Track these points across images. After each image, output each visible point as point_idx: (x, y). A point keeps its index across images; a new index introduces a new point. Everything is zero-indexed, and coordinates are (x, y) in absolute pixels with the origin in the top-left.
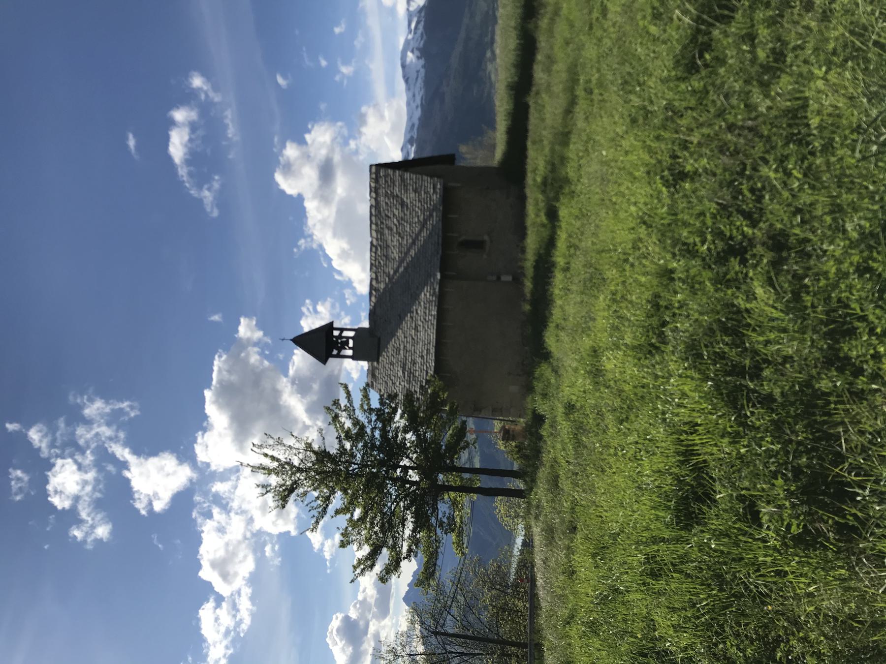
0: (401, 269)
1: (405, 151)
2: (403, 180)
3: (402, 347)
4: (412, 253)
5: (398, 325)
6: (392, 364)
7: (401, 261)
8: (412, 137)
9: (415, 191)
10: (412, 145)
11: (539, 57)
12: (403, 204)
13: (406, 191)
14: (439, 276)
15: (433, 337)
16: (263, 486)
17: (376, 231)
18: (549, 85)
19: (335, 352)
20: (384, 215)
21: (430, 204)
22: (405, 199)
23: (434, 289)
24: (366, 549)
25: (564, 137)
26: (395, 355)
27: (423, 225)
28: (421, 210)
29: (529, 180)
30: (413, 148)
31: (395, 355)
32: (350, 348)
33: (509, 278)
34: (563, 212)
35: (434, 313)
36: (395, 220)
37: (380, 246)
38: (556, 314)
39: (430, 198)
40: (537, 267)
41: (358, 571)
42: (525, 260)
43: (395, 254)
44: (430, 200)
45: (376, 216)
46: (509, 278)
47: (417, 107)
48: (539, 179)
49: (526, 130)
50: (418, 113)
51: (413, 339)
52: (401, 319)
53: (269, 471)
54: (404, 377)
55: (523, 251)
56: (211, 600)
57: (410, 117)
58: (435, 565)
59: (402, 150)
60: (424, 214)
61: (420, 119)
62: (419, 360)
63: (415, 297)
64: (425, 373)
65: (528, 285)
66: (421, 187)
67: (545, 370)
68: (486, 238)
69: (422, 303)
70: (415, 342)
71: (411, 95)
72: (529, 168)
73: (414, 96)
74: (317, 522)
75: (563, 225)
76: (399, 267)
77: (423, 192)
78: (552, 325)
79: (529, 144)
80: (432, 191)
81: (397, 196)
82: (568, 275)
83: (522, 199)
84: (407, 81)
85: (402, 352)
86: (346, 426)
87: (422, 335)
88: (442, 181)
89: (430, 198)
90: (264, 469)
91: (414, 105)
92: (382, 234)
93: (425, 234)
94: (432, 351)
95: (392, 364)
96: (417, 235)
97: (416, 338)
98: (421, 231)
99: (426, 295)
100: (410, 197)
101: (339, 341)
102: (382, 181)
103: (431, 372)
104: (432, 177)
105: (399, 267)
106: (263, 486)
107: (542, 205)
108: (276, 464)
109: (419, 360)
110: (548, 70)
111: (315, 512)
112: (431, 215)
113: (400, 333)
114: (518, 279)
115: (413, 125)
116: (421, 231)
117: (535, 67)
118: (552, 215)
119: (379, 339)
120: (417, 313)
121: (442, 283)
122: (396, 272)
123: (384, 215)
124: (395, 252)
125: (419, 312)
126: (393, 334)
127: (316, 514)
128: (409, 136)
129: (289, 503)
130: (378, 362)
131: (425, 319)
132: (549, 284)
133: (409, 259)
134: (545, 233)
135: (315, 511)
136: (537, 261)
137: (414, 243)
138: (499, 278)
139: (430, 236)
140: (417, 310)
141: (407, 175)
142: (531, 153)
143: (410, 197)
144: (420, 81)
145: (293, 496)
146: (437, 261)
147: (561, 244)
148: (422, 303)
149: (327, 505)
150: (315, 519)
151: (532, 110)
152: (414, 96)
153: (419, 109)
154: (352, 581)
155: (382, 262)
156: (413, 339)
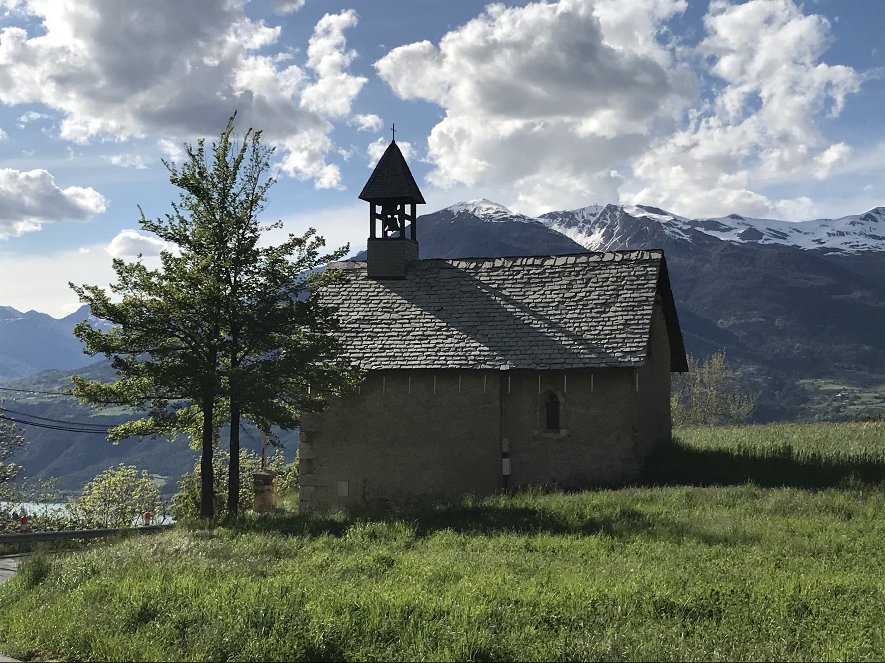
0: (510, 308)
1: (730, 223)
2: (641, 303)
3: (394, 316)
4: (537, 324)
5: (425, 307)
6: (367, 301)
7: (523, 308)
8: (760, 235)
9: (626, 324)
10: (742, 236)
11: (800, 495)
12: (607, 305)
13: (625, 310)
14: (503, 368)
15: (414, 365)
16: (200, 150)
17: (566, 264)
18: (758, 511)
19: (379, 210)
20: (589, 276)
21: (608, 348)
22: (613, 309)
23: (485, 362)
24: (116, 299)
25: (679, 532)
26: (382, 305)
27: (578, 338)
28: (599, 334)
29: (642, 493)
30: (737, 239)
31: (382, 305)
32: (385, 233)
33: (506, 470)
34: (593, 540)
35: (451, 364)
36: (583, 294)
37: (544, 272)
38: (478, 541)
39: (617, 348)
40: (529, 513)
41: (87, 293)
42: (535, 496)
43: (533, 297)
44: (613, 348)
45: (588, 263)
46: (506, 470)
47: (819, 241)
48: (638, 507)
49: (706, 484)
50: (807, 244)
51: (409, 332)
52: (438, 312)
53: (221, 159)
54: (349, 323)
55: (547, 491)
56: (120, 157)
57: (797, 229)
58: (108, 402)
59: (734, 217)
60: (592, 340)
61: (796, 247)
62: (378, 344)
63: (471, 332)
64: (361, 355)
65: (503, 502)
66: (633, 333)
67: (406, 533)
68: (563, 432)
69: (462, 344)
70: (403, 336)
71: (842, 227)
72: (656, 491)
73: (842, 234)
74: (155, 229)
75: (579, 542)
76: (514, 303)
77: (624, 336)
78: (461, 538)
79: (689, 489)
80: (628, 349)
81: (618, 295)
82: (524, 550)
83: (615, 485)
84: (868, 217)
85: (387, 316)
86: (287, 257)
87: (415, 346)
88: (641, 364)
89: (617, 348)
90: (225, 149)
91: (822, 235)
92: (561, 274)
93: (565, 341)
94: (394, 365)
95: (367, 301)
96: (562, 330)
97: (409, 337)
98: (569, 335)
99: (476, 349)
100: (616, 315)
101: (396, 216)
102: (639, 270)
103: (365, 366)
104: (649, 348)
105: (514, 303)
106: (200, 150)
107: (607, 512)
108: (231, 165)
109: (378, 344)
110: (781, 511)
111: (166, 223)
112: (591, 349)
113: (415, 311)
114: (509, 486)
115: (784, 236)
116: (569, 335)
117: (787, 491)
118: (590, 528)
119: (403, 278)
120: (448, 337)
121: (495, 372)
122: (507, 299)
123: (589, 276)
124: (536, 296)
125: (450, 340)
126: (412, 300)
127: (163, 226)
128: (761, 228)
129: (179, 188)
130: (367, 278)
131: (439, 351)
132: (510, 529)
133: (526, 318)
134: (573, 519)
135: (168, 224)
136: (534, 512)
137: (552, 325)
138: (505, 455)
139: (562, 350)
140: (451, 336)
141: (648, 310)
142: (676, 493)
143: (616, 315)
144: (872, 243)
145: (186, 192)
146: (526, 364)
147: (556, 541)
148: (462, 344)
149: (176, 241)
150: (156, 223)
151: (732, 490)
152: (842, 234)
153: (815, 246)
154: (72, 285)
155: (519, 276)
156: (409, 332)
